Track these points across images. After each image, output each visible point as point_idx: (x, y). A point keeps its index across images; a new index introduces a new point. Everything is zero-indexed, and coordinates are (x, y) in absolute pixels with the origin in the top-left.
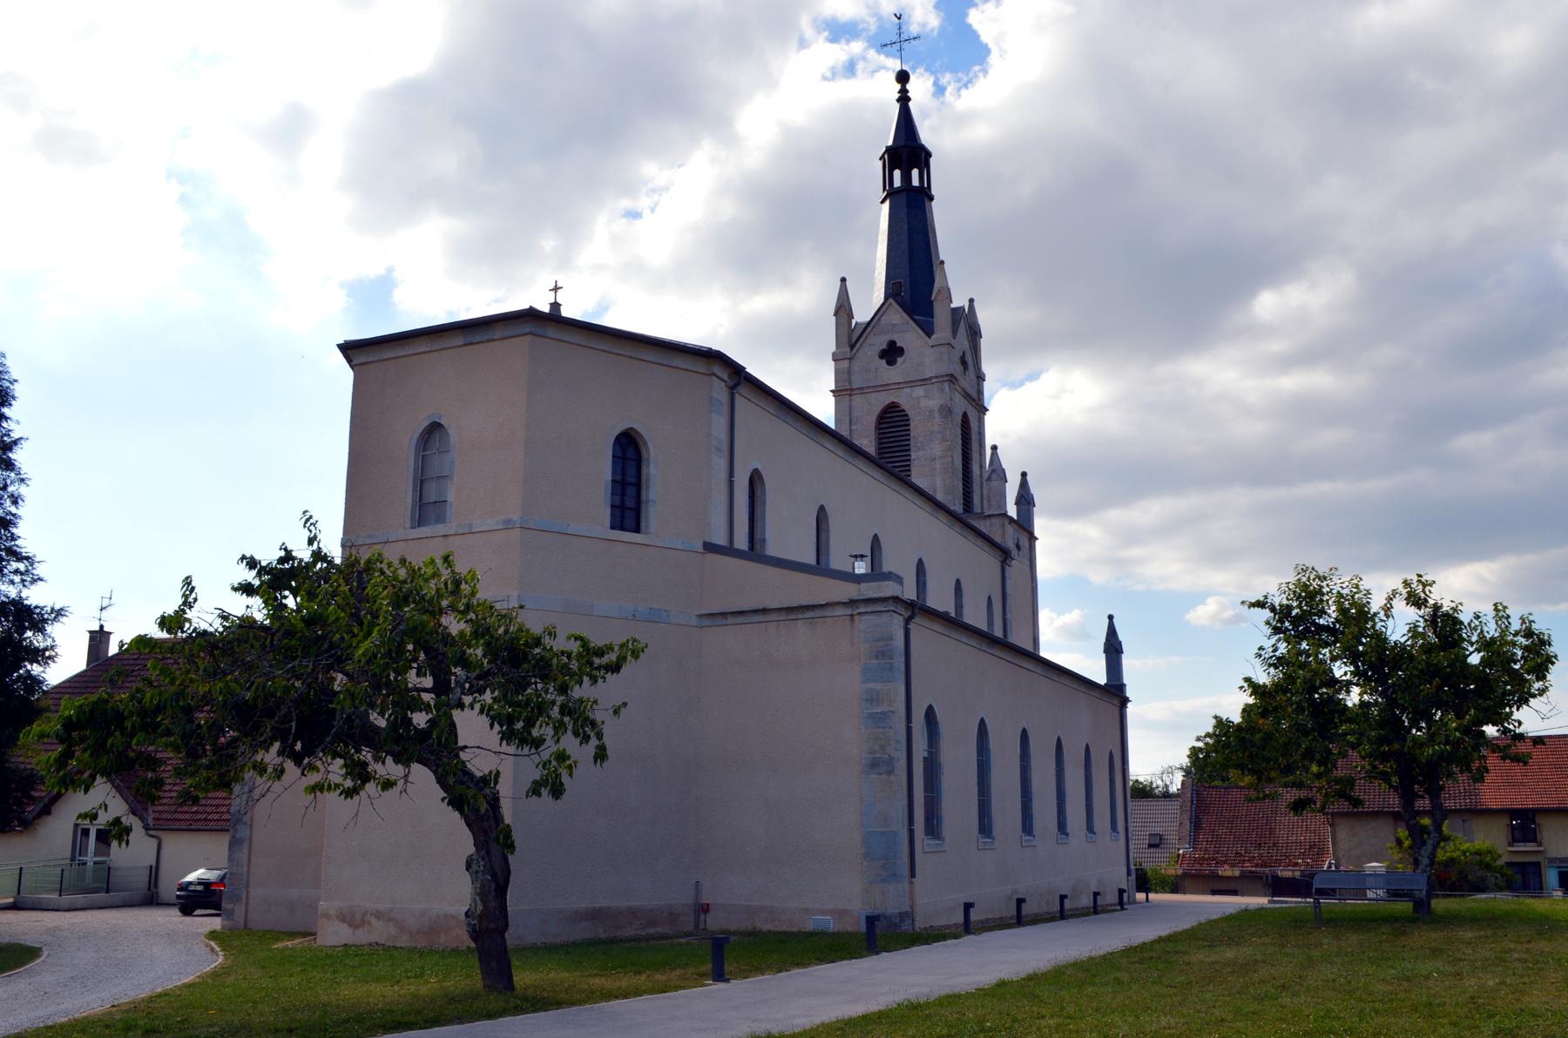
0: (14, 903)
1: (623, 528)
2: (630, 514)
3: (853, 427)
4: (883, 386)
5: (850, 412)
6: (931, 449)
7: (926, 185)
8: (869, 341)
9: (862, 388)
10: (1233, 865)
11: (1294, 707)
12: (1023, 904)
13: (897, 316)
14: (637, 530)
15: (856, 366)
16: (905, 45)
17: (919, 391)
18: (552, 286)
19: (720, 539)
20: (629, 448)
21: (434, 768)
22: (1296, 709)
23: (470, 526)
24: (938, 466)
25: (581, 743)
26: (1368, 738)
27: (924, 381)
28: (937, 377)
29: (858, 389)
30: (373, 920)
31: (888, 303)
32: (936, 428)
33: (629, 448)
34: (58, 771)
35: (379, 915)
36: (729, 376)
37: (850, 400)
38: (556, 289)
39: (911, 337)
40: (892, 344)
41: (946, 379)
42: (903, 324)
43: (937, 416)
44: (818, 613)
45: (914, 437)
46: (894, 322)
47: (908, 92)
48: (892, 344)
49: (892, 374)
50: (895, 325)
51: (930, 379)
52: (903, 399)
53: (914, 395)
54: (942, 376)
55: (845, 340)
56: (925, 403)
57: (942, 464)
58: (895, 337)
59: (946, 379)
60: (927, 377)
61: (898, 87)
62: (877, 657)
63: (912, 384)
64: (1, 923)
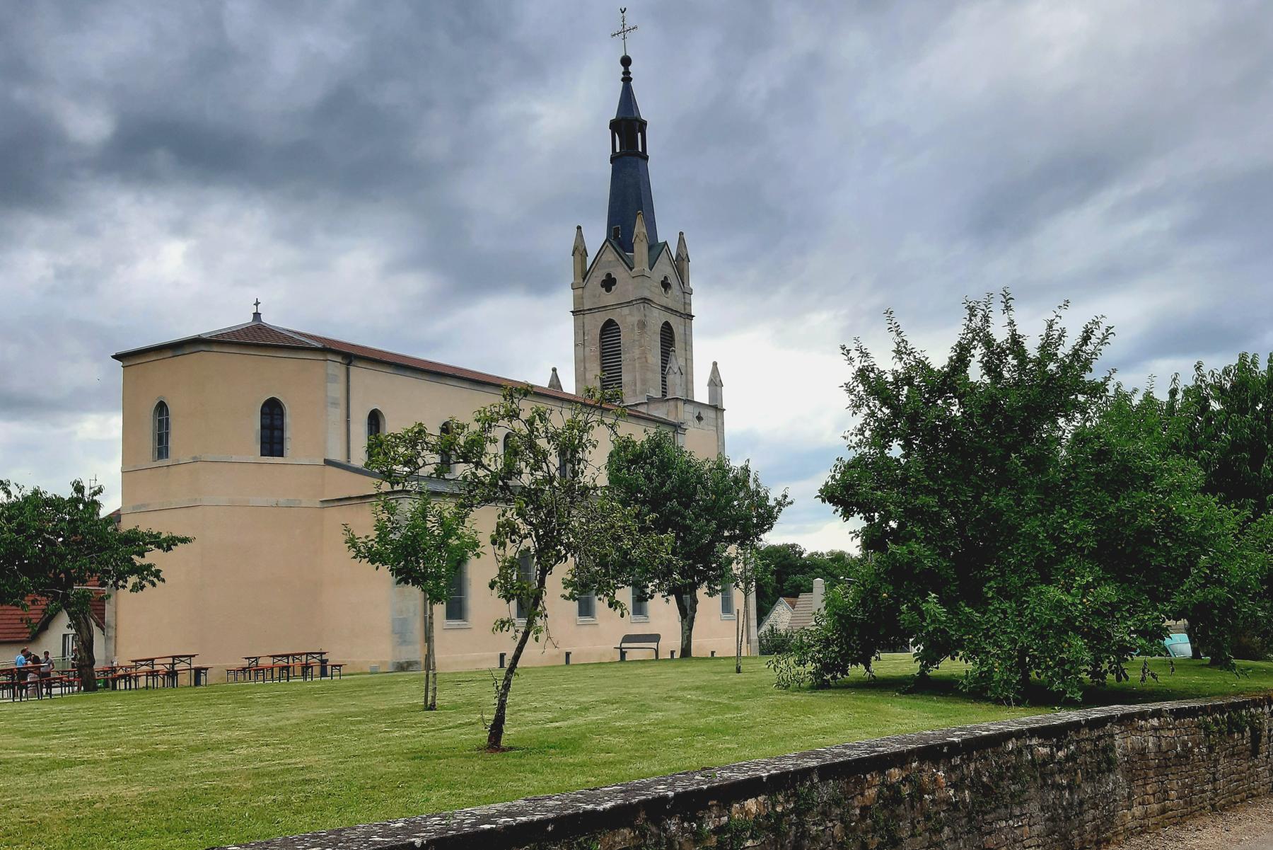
1: (272, 455)
2: (277, 447)
3: (586, 338)
5: (584, 326)
6: (633, 352)
7: (640, 150)
8: (594, 274)
9: (591, 309)
12: (570, 655)
13: (610, 255)
14: (282, 455)
15: (587, 292)
16: (627, 34)
17: (626, 311)
18: (255, 302)
19: (338, 456)
21: (1196, 645)
23: (178, 461)
25: (398, 583)
26: (917, 539)
28: (636, 300)
29: (588, 310)
31: (606, 246)
32: (636, 338)
36: (342, 360)
37: (584, 318)
38: (257, 304)
39: (620, 273)
40: (609, 275)
47: (630, 73)
48: (609, 275)
49: (609, 298)
50: (610, 262)
53: (623, 314)
54: (639, 299)
55: (579, 272)
56: (629, 319)
58: (610, 270)
61: (622, 69)
63: (621, 305)
64: (1, 748)
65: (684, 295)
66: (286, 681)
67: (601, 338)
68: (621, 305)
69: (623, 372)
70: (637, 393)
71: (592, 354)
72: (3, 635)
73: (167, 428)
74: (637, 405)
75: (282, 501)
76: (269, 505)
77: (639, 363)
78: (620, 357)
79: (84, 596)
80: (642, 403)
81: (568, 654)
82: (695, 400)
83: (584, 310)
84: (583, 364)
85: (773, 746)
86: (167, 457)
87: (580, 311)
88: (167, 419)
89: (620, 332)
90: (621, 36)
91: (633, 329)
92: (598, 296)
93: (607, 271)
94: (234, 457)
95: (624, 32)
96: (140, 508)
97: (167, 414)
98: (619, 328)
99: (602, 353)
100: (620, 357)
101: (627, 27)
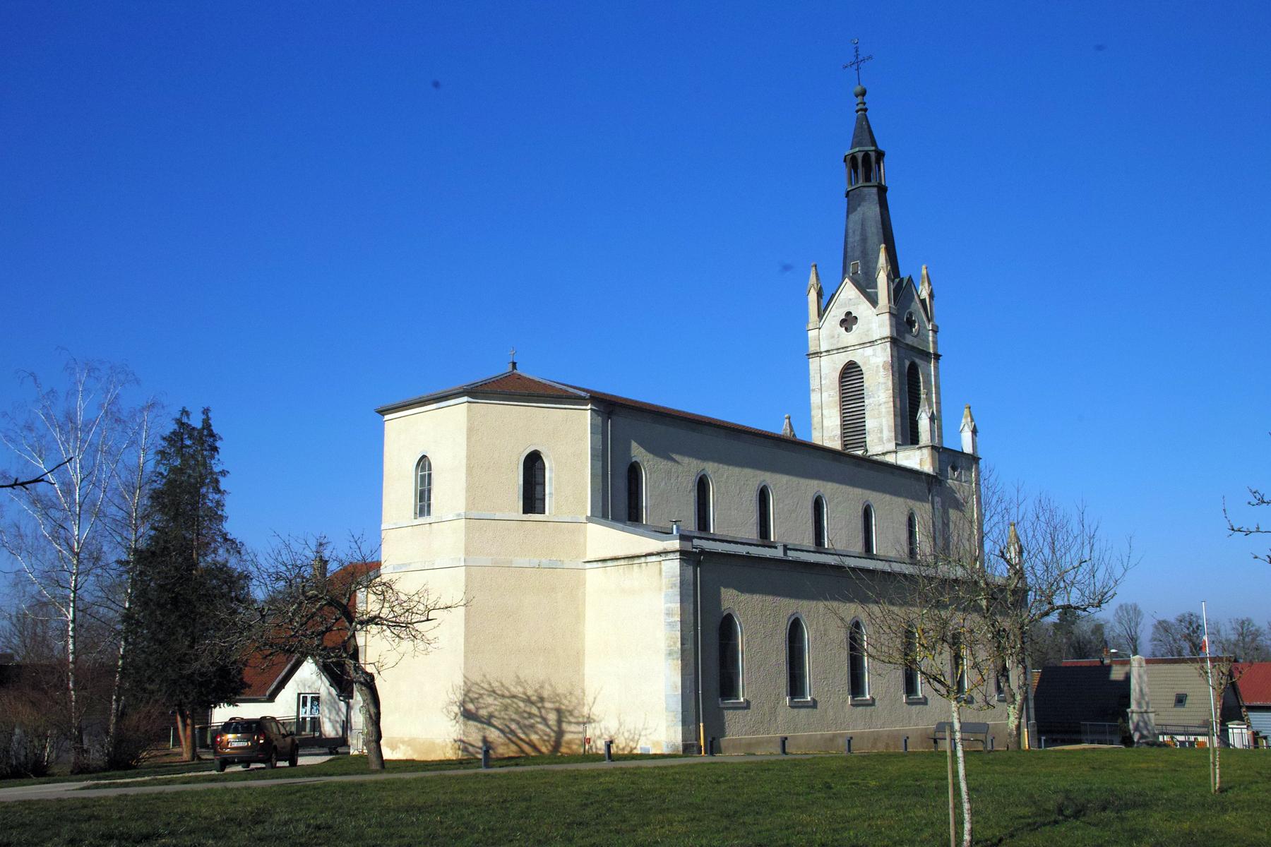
0: (383, 415)
4: (843, 348)
10: (294, 610)
11: (173, 595)
20: (533, 464)
22: (172, 598)
23: (441, 518)
24: (884, 410)
27: (872, 343)
29: (826, 351)
30: (401, 746)
33: (533, 464)
34: (31, 777)
35: (403, 742)
39: (862, 309)
40: (849, 314)
41: (887, 340)
42: (856, 298)
43: (881, 370)
44: (643, 560)
45: (866, 388)
46: (849, 297)
48: (849, 314)
51: (876, 341)
52: (857, 356)
54: (884, 338)
57: (886, 408)
59: (887, 340)
60: (874, 340)
62: (672, 587)
63: (863, 345)
65: (24, 487)
66: (287, 764)
67: (841, 382)
68: (863, 345)
69: (866, 416)
70: (885, 442)
71: (831, 399)
72: (1269, 721)
73: (430, 484)
74: (884, 454)
75: (545, 562)
76: (532, 565)
77: (886, 408)
78: (864, 402)
79: (1201, 648)
80: (890, 452)
81: (784, 740)
82: (945, 446)
83: (821, 353)
84: (820, 411)
85: (398, 817)
86: (429, 513)
87: (817, 353)
88: (430, 475)
89: (862, 374)
90: (855, 66)
91: (877, 372)
92: (836, 336)
93: (847, 310)
94: (497, 514)
95: (857, 63)
96: (401, 568)
97: (430, 469)
98: (861, 370)
99: (841, 398)
100: (864, 402)
101: (860, 58)
